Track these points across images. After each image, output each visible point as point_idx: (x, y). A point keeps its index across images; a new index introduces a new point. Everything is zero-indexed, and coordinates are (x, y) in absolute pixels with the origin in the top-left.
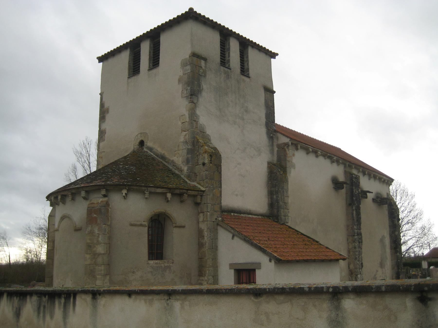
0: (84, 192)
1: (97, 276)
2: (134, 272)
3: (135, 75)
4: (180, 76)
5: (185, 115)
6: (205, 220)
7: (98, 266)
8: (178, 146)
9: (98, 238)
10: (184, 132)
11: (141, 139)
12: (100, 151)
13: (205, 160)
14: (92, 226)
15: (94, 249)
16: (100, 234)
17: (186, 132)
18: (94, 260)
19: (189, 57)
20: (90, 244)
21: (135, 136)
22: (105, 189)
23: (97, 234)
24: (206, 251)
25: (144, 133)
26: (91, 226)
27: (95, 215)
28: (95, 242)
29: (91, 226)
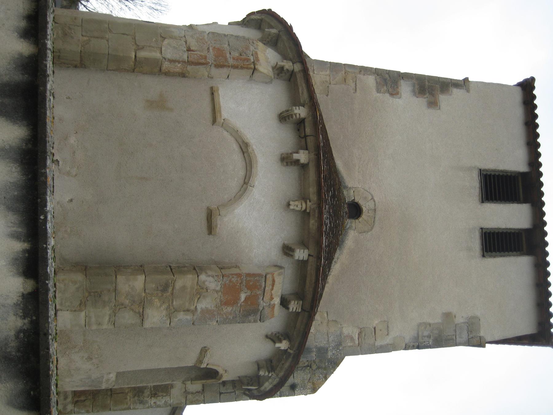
0: (306, 258)
1: (83, 314)
2: (91, 359)
3: (481, 190)
4: (455, 317)
5: (388, 335)
6: (188, 398)
7: (110, 315)
8: (336, 321)
9: (184, 311)
10: (359, 334)
11: (364, 209)
12: (359, 76)
13: (301, 390)
14: (217, 292)
15: (157, 302)
16: (194, 315)
17: (358, 337)
18: (127, 302)
19: (480, 337)
20: (170, 289)
21: (373, 193)
22: (300, 311)
23: (196, 307)
24: (127, 404)
25: (375, 218)
26: (218, 288)
27: (243, 296)
28: (174, 303)
29: (218, 288)
